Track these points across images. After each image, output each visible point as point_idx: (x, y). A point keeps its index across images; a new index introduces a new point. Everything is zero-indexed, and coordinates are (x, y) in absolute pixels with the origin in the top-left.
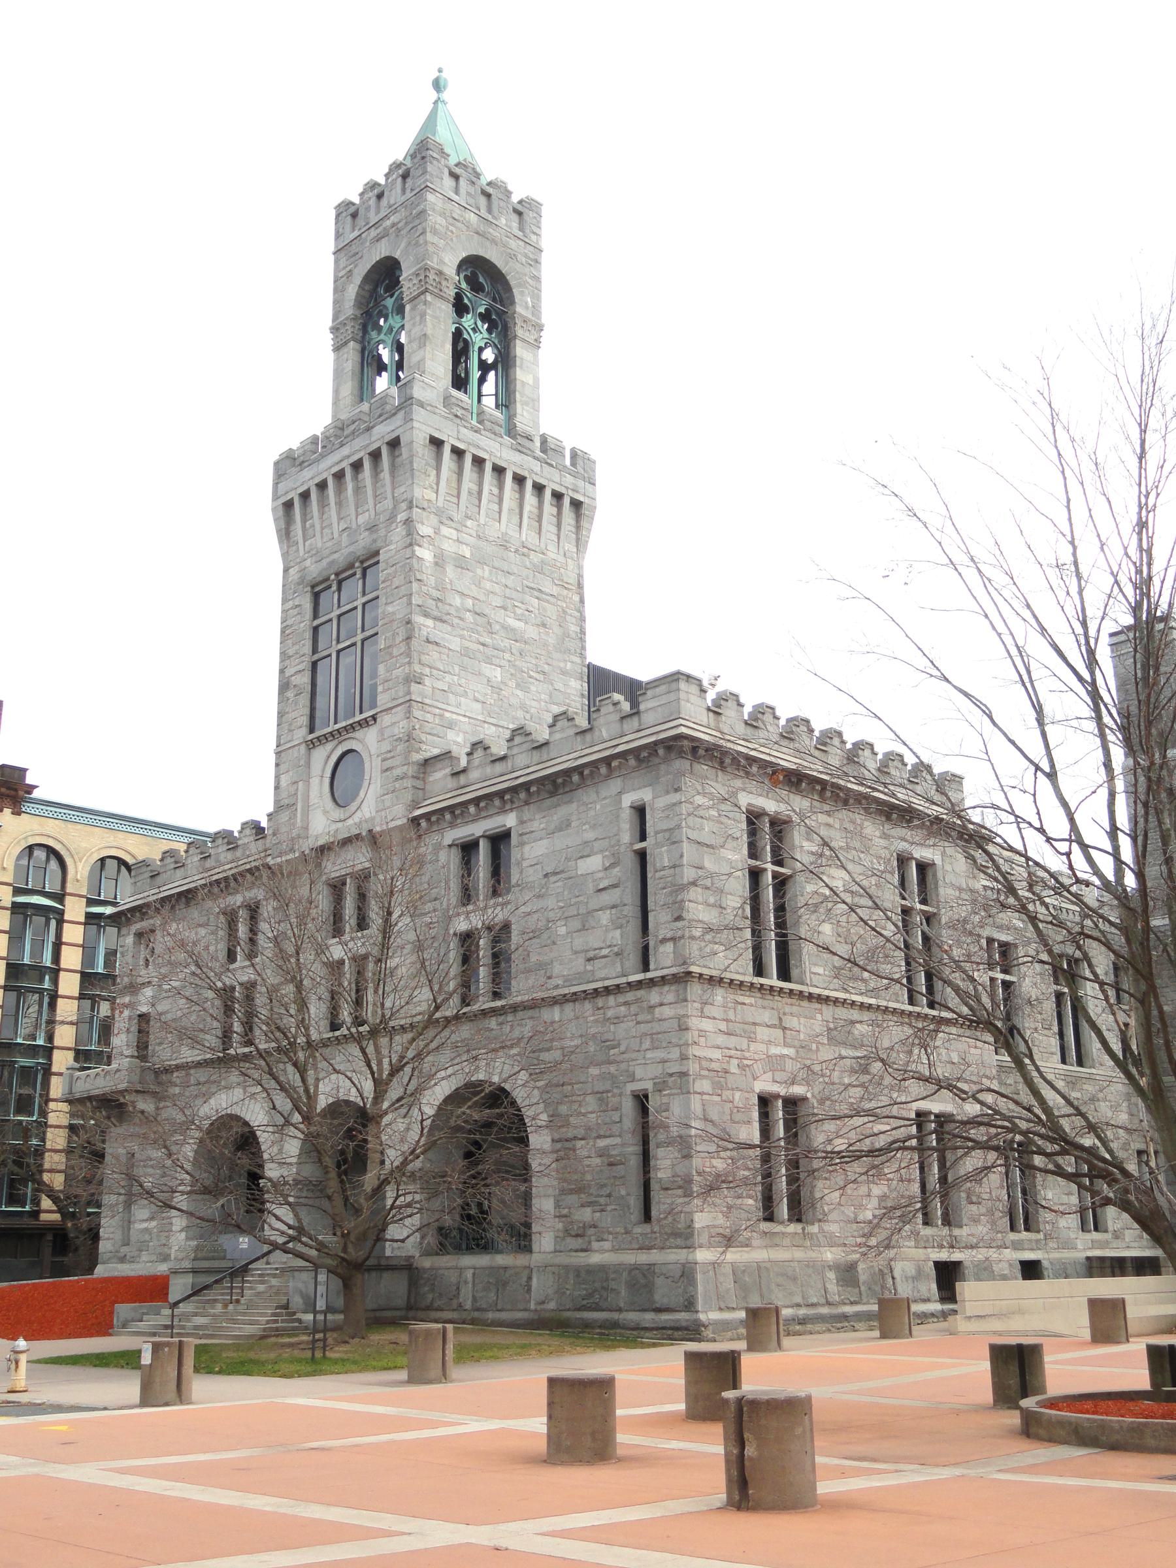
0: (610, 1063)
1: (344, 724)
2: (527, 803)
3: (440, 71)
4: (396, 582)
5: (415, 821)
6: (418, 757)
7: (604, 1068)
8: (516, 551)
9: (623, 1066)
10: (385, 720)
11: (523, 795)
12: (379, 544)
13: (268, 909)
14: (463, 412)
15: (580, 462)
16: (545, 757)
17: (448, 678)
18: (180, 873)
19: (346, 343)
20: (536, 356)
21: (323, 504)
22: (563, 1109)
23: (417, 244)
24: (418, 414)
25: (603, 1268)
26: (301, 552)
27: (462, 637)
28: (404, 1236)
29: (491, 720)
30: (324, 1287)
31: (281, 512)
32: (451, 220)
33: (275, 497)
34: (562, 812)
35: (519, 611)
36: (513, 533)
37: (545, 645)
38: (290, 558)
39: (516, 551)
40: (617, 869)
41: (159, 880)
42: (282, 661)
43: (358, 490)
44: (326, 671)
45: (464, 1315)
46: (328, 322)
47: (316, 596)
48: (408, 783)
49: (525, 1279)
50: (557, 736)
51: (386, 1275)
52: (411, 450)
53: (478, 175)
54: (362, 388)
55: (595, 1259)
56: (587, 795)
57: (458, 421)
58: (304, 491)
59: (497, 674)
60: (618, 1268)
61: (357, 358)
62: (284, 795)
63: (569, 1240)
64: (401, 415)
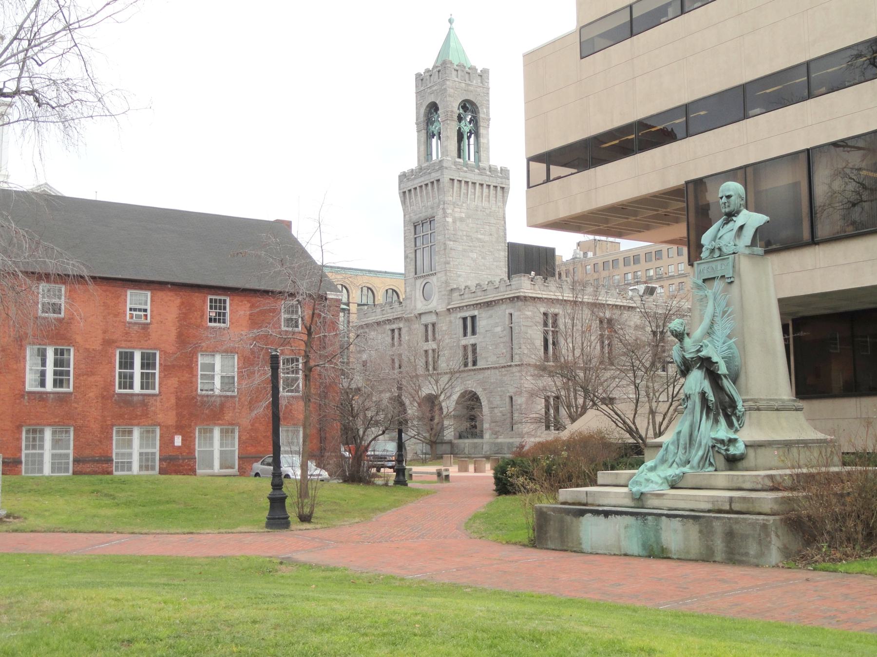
5: (449, 310)
6: (449, 288)
10: (439, 275)
13: (404, 331)
21: (416, 195)
25: (501, 443)
28: (449, 434)
30: (426, 448)
33: (400, 189)
34: (490, 312)
43: (427, 193)
47: (415, 227)
53: (465, 67)
56: (497, 308)
58: (411, 187)
59: (475, 256)
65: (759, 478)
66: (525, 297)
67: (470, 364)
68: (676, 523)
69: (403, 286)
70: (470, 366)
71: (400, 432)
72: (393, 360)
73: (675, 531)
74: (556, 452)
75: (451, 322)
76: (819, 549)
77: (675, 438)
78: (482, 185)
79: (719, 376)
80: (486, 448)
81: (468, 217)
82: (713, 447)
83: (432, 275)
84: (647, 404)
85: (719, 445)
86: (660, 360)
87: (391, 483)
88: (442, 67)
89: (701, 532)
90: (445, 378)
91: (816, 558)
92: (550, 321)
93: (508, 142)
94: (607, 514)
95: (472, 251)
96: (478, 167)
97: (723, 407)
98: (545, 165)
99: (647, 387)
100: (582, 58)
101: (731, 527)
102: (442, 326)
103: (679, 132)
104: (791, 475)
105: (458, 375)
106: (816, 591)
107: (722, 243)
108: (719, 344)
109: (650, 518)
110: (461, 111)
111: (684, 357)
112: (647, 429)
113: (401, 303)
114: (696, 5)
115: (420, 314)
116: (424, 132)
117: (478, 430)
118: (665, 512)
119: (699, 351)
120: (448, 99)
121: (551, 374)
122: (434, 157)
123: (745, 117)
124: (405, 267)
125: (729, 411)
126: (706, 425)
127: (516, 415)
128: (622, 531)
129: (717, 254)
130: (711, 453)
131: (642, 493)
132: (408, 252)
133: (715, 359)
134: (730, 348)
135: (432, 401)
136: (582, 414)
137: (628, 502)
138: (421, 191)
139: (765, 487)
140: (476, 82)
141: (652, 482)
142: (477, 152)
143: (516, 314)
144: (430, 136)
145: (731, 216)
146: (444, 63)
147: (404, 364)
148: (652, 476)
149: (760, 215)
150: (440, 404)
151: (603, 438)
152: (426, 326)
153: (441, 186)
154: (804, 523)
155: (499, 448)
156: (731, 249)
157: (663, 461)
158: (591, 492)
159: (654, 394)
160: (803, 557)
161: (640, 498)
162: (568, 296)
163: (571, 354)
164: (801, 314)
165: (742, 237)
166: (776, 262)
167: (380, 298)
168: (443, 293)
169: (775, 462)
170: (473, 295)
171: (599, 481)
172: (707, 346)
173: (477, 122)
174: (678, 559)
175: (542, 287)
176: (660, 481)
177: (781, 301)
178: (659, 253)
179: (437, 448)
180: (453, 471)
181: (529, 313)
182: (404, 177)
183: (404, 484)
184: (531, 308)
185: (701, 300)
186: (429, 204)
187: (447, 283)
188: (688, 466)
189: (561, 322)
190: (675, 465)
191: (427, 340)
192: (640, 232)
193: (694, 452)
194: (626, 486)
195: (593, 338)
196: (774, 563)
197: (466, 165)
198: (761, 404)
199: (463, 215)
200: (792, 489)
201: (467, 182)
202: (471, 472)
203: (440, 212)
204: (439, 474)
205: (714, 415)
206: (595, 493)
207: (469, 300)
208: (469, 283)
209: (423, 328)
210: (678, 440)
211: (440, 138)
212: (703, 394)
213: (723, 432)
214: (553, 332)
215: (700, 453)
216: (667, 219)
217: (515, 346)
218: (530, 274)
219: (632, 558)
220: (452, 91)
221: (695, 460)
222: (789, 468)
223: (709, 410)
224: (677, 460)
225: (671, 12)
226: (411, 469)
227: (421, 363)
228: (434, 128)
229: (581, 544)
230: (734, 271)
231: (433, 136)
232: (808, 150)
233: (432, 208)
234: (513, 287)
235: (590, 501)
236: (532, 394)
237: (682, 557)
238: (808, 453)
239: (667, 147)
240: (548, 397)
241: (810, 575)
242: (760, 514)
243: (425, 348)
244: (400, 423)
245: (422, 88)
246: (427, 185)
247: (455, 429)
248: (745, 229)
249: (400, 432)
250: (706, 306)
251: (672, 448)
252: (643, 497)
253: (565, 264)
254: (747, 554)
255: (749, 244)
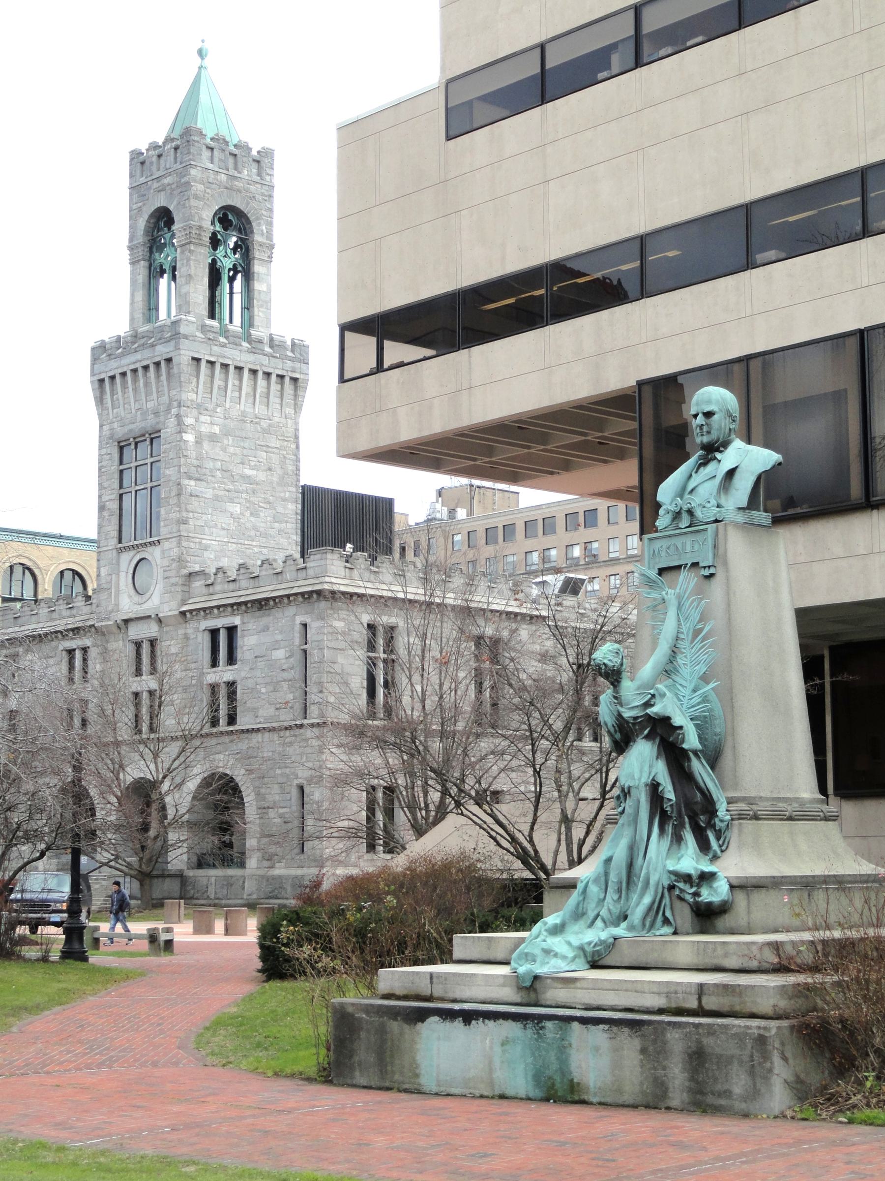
0: (286, 768)
1: (140, 542)
2: (246, 612)
3: (203, 41)
4: (172, 455)
5: (183, 613)
7: (284, 770)
8: (251, 422)
9: (292, 770)
10: (166, 545)
11: (243, 608)
12: (160, 426)
13: (93, 653)
14: (214, 335)
15: (297, 349)
16: (257, 585)
17: (204, 517)
18: (34, 618)
19: (139, 261)
20: (269, 269)
21: (124, 386)
22: (263, 791)
23: (184, 206)
24: (184, 344)
25: (280, 877)
26: (111, 417)
27: (214, 488)
28: (178, 859)
29: (233, 540)
31: (96, 385)
32: (208, 185)
33: (93, 374)
35: (253, 464)
36: (249, 410)
37: (272, 482)
38: (104, 418)
39: (251, 422)
40: (292, 659)
41: (20, 621)
42: (100, 490)
43: (147, 384)
44: (128, 500)
45: (210, 902)
46: (126, 242)
47: (121, 448)
48: (179, 589)
49: (241, 882)
50: (264, 573)
51: (168, 880)
52: (179, 369)
53: (227, 143)
54: (150, 295)
55: (277, 872)
57: (211, 342)
58: (128, 370)
59: (236, 509)
60: (287, 877)
61: (146, 272)
62: (103, 581)
63: (265, 862)
64: (173, 343)
65: (754, 948)
66: (333, 593)
67: (223, 721)
68: (598, 1035)
69: (95, 564)
70: (223, 726)
71: (76, 855)
72: (70, 711)
73: (597, 1049)
74: (377, 899)
75: (186, 637)
76: (860, 1083)
77: (601, 870)
78: (254, 372)
79: (684, 752)
80: (250, 886)
81: (227, 433)
82: (671, 888)
83: (152, 544)
84: (558, 805)
85: (681, 885)
86: (584, 720)
87: (55, 955)
88: (183, 141)
89: (643, 1051)
90: (173, 749)
91: (854, 1100)
92: (381, 641)
93: (304, 292)
94: (468, 1017)
95: (232, 501)
96: (248, 338)
97: (690, 812)
98: (373, 340)
99: (558, 771)
100: (449, 138)
101: (699, 1042)
102: (170, 646)
103: (631, 286)
104: (812, 942)
105: (197, 742)
106: (848, 1163)
107: (695, 501)
108: (686, 692)
109: (549, 1024)
110: (218, 227)
111: (620, 715)
112: (556, 852)
113: (88, 598)
114: (663, 52)
115: (126, 621)
116: (143, 264)
117: (235, 852)
118: (579, 1013)
119: (648, 705)
120: (193, 202)
121: (381, 744)
122: (163, 314)
123: (750, 264)
124: (100, 527)
125: (702, 820)
126: (658, 846)
127: (309, 822)
128: (498, 1049)
129: (685, 521)
130: (667, 900)
131: (536, 978)
132: (105, 498)
133: (677, 721)
134: (705, 699)
135: (144, 793)
136: (436, 823)
137: (508, 993)
138: (135, 380)
139: (766, 966)
140: (248, 172)
141: (556, 955)
142: (247, 307)
143: (313, 626)
144: (155, 272)
145: (712, 450)
146: (187, 133)
147: (92, 716)
148: (557, 943)
149: (766, 452)
150: (161, 799)
151: (472, 868)
152: (138, 645)
153: (175, 370)
154: (833, 1033)
155: (275, 887)
156: (712, 513)
157: (578, 915)
158: (439, 975)
159: (570, 785)
160: (831, 1099)
161: (532, 986)
162: (415, 592)
163: (418, 706)
164: (845, 639)
165: (733, 491)
166: (797, 540)
167: (47, 588)
168: (174, 580)
169: (784, 917)
170: (232, 586)
171: (457, 954)
172: (663, 695)
173: (248, 250)
174: (600, 1104)
175: (367, 575)
176: (571, 954)
177: (803, 615)
178: (591, 517)
179: (152, 886)
180: (183, 932)
181: (339, 625)
182: (100, 351)
183: (82, 957)
184: (343, 614)
185: (654, 608)
186: (150, 405)
187: (181, 561)
188: (624, 925)
189: (401, 643)
190: (599, 923)
191: (138, 672)
192: (552, 473)
193: (635, 897)
194: (507, 963)
195: (461, 675)
196: (776, 1112)
197: (225, 332)
198: (761, 807)
199: (217, 430)
200: (814, 969)
201: (225, 366)
202: (218, 934)
203: (172, 421)
204: (153, 938)
205: (675, 827)
206: (447, 976)
207: (223, 595)
208: (224, 562)
209: (130, 649)
210: (606, 874)
211: (174, 278)
212: (654, 788)
213: (689, 860)
214: (385, 661)
215: (647, 900)
216: (605, 451)
217: (312, 689)
218: (343, 547)
219: (513, 1103)
220: (201, 187)
221: (637, 914)
222: (809, 929)
223: (664, 818)
224: (604, 912)
225: (616, 60)
226: (97, 929)
227: (125, 717)
228: (164, 258)
229: (417, 1076)
230: (715, 556)
231: (162, 272)
232: (861, 332)
233: (156, 413)
234: (311, 572)
235: (438, 992)
236: (341, 781)
237: (608, 1100)
238: (844, 901)
239: (604, 315)
240: (374, 788)
241: (845, 1132)
242: (753, 1016)
243: (135, 688)
244: (76, 837)
245: (143, 180)
246: (146, 368)
247: (190, 849)
248: (737, 476)
249: (76, 855)
250: (663, 621)
251: (594, 890)
252: (538, 985)
253: (410, 530)
254: (727, 1093)
255: (744, 504)
